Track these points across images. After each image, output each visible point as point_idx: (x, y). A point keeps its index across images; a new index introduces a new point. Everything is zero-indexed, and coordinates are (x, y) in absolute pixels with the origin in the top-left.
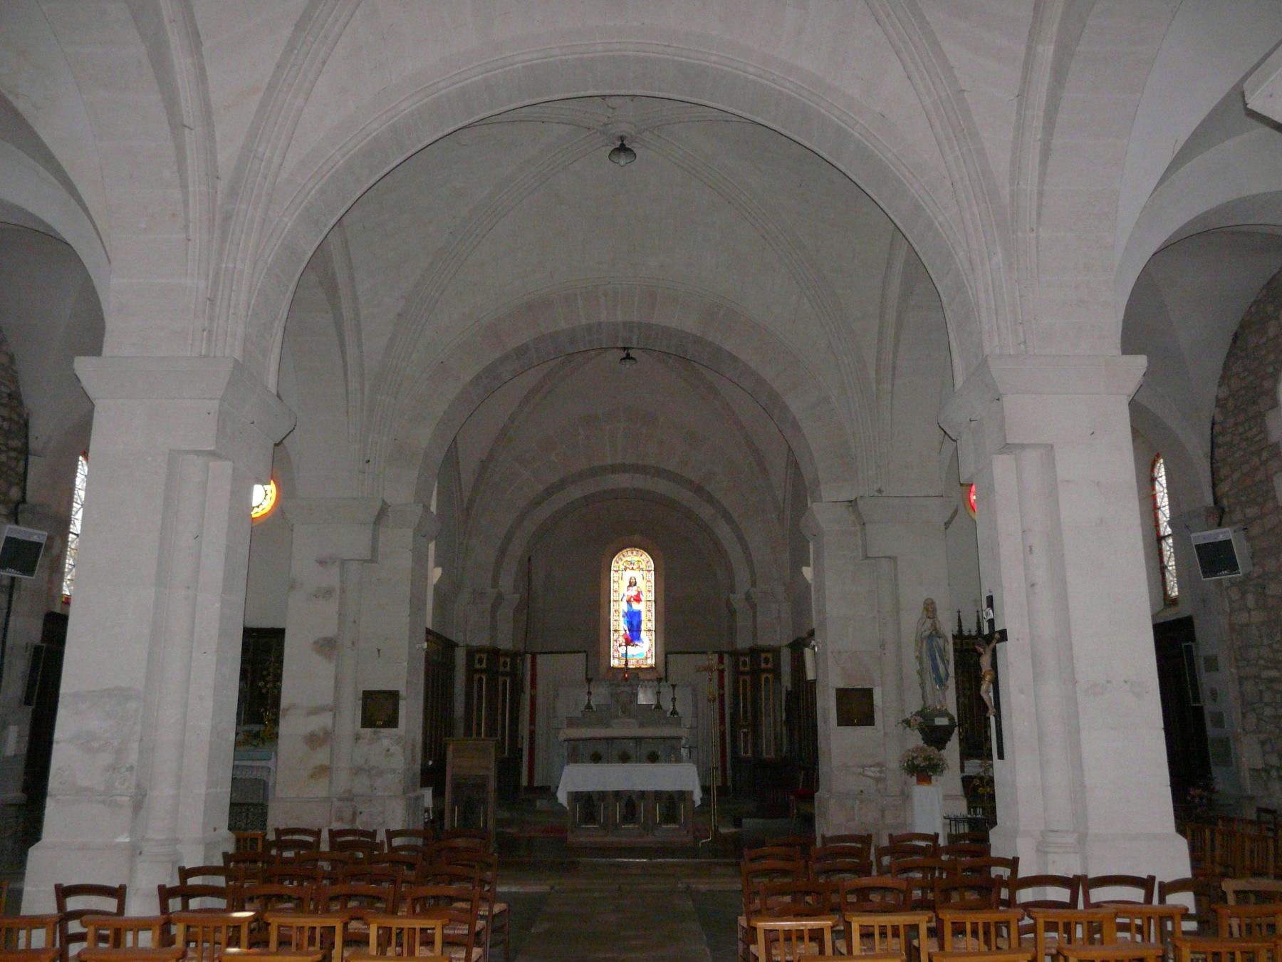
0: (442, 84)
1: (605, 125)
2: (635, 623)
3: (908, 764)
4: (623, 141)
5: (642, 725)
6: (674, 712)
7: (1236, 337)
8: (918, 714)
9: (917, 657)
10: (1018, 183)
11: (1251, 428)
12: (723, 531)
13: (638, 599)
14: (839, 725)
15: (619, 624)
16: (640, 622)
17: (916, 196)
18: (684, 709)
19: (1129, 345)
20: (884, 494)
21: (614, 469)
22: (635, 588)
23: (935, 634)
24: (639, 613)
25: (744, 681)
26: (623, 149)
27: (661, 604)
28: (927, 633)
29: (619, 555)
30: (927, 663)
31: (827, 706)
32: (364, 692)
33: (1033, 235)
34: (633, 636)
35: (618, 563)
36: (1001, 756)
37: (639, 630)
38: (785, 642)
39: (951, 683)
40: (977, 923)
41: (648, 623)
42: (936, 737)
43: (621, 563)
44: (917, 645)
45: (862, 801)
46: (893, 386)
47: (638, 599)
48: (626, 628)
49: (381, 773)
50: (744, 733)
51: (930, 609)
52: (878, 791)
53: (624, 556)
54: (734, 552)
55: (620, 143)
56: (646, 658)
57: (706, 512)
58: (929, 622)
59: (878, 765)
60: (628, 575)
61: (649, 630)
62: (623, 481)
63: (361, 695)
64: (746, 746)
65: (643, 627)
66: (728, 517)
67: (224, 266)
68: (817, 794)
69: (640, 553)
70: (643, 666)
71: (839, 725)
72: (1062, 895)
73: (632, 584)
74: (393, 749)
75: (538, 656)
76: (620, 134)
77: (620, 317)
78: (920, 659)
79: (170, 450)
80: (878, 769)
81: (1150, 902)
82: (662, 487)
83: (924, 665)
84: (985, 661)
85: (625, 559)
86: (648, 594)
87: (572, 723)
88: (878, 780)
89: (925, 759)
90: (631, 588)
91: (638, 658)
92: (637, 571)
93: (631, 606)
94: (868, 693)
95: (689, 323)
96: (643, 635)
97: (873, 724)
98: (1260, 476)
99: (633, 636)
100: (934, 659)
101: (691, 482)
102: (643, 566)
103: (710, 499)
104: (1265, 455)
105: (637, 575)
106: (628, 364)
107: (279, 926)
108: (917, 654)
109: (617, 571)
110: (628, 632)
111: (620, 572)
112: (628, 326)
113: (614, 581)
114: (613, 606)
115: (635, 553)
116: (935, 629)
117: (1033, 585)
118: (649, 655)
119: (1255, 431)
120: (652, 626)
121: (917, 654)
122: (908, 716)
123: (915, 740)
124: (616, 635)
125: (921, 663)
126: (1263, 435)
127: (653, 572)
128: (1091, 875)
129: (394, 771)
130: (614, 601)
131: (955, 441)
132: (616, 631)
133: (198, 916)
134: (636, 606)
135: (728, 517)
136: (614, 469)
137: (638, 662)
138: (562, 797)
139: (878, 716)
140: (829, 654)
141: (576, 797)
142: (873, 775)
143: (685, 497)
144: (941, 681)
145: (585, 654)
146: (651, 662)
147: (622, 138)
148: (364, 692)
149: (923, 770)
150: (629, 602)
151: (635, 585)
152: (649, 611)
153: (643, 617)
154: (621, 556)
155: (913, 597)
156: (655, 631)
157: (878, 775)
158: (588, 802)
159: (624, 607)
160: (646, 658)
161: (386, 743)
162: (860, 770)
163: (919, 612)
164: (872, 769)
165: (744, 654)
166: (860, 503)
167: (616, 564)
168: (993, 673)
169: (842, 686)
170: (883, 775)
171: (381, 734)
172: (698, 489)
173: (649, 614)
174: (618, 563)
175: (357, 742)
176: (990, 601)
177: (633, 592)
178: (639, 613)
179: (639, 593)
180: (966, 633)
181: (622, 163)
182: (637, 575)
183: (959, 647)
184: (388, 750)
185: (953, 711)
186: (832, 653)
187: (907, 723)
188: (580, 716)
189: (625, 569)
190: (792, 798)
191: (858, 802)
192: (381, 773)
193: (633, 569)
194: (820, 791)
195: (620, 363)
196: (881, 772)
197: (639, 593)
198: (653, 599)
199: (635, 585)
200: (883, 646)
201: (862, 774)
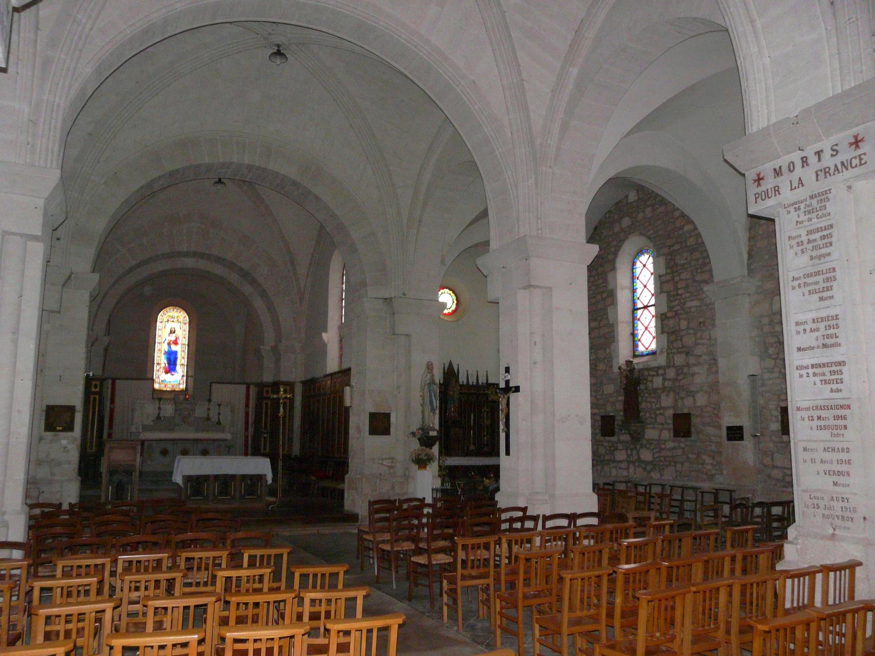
0: (476, 107)
1: (270, 34)
2: (172, 359)
3: (416, 459)
4: (279, 47)
5: (197, 431)
6: (219, 423)
7: (596, 228)
8: (419, 429)
9: (421, 396)
10: (547, 140)
11: (598, 279)
12: (258, 303)
13: (176, 343)
14: (370, 434)
15: (160, 359)
16: (176, 359)
17: (488, 134)
18: (226, 418)
19: (591, 240)
20: (407, 296)
21: (187, 254)
22: (174, 335)
23: (432, 382)
24: (176, 352)
25: (266, 404)
26: (279, 53)
27: (193, 348)
28: (428, 382)
29: (164, 311)
30: (427, 399)
31: (359, 422)
32: (48, 407)
33: (551, 170)
34: (171, 367)
35: (162, 316)
36: (508, 453)
37: (175, 364)
38: (299, 380)
39: (437, 412)
40: (512, 540)
41: (182, 359)
42: (426, 441)
43: (165, 317)
44: (421, 387)
45: (380, 479)
46: (418, 231)
47: (176, 343)
48: (166, 362)
49: (59, 464)
50: (265, 438)
51: (430, 367)
52: (390, 473)
53: (167, 312)
54: (265, 317)
55: (277, 48)
56: (179, 384)
57: (247, 289)
58: (429, 376)
59: (392, 458)
60: (170, 325)
61: (183, 365)
62: (190, 263)
63: (45, 408)
64: (265, 445)
65: (178, 362)
66: (264, 294)
67: (45, 98)
68: (347, 476)
69: (179, 311)
70: (177, 390)
71: (370, 434)
72: (564, 522)
73: (172, 332)
74: (70, 447)
75: (117, 381)
76: (278, 43)
77: (247, 160)
78: (423, 397)
79: (3, 232)
80: (391, 461)
81: (570, 527)
82: (218, 270)
83: (426, 401)
84: (503, 406)
85: (168, 314)
86: (183, 340)
87: (146, 428)
88: (390, 467)
89: (426, 455)
90: (171, 335)
91: (173, 383)
92: (176, 323)
93: (170, 347)
94: (388, 416)
95: (290, 171)
96: (178, 368)
97: (389, 434)
98: (600, 306)
99: (171, 367)
100: (431, 396)
101: (241, 269)
102: (181, 320)
103: (253, 282)
104: (604, 295)
105: (176, 326)
106: (219, 186)
107: (63, 567)
108: (422, 394)
109: (161, 322)
110: (167, 365)
111: (164, 323)
112: (250, 168)
113: (159, 329)
114: (157, 347)
115: (175, 310)
116: (433, 380)
117: (535, 363)
118: (181, 382)
119: (601, 281)
120: (185, 361)
121: (422, 394)
122: (415, 430)
123: (415, 445)
124: (158, 367)
125: (423, 400)
126: (605, 284)
127: (187, 325)
128: (578, 513)
129: (69, 462)
130: (158, 343)
131: (486, 276)
132: (158, 364)
133: (550, 531)
134: (174, 348)
135: (264, 294)
136: (187, 254)
137: (173, 386)
138: (178, 479)
139: (392, 429)
140: (367, 392)
141: (188, 479)
142: (388, 464)
143: (234, 277)
144: (433, 410)
145: (214, 386)
146: (183, 387)
147: (278, 46)
148: (48, 407)
149: (422, 462)
150: (169, 344)
151: (174, 333)
152: (183, 351)
153: (179, 356)
154: (165, 312)
155: (419, 360)
156: (187, 366)
157: (390, 464)
158: (196, 483)
159: (165, 347)
160: (179, 384)
161: (64, 442)
162: (381, 462)
163: (423, 369)
164: (387, 461)
165: (268, 386)
166: (394, 300)
167: (161, 317)
168: (507, 409)
169: (373, 410)
170: (393, 464)
171: (60, 436)
172: (245, 275)
173: (183, 354)
174: (162, 316)
175: (40, 442)
176: (507, 370)
177: (173, 337)
178: (176, 352)
179: (177, 339)
180: (471, 383)
181: (278, 63)
182: (176, 326)
183: (443, 390)
184: (65, 448)
185: (437, 427)
186: (369, 391)
187: (413, 434)
188: (152, 424)
189: (168, 321)
190: (313, 478)
191: (378, 480)
192: (59, 464)
193: (173, 321)
194: (349, 473)
195: (214, 185)
196: (392, 462)
197: (177, 339)
198: (187, 343)
199: (174, 333)
200: (399, 387)
201: (382, 464)
